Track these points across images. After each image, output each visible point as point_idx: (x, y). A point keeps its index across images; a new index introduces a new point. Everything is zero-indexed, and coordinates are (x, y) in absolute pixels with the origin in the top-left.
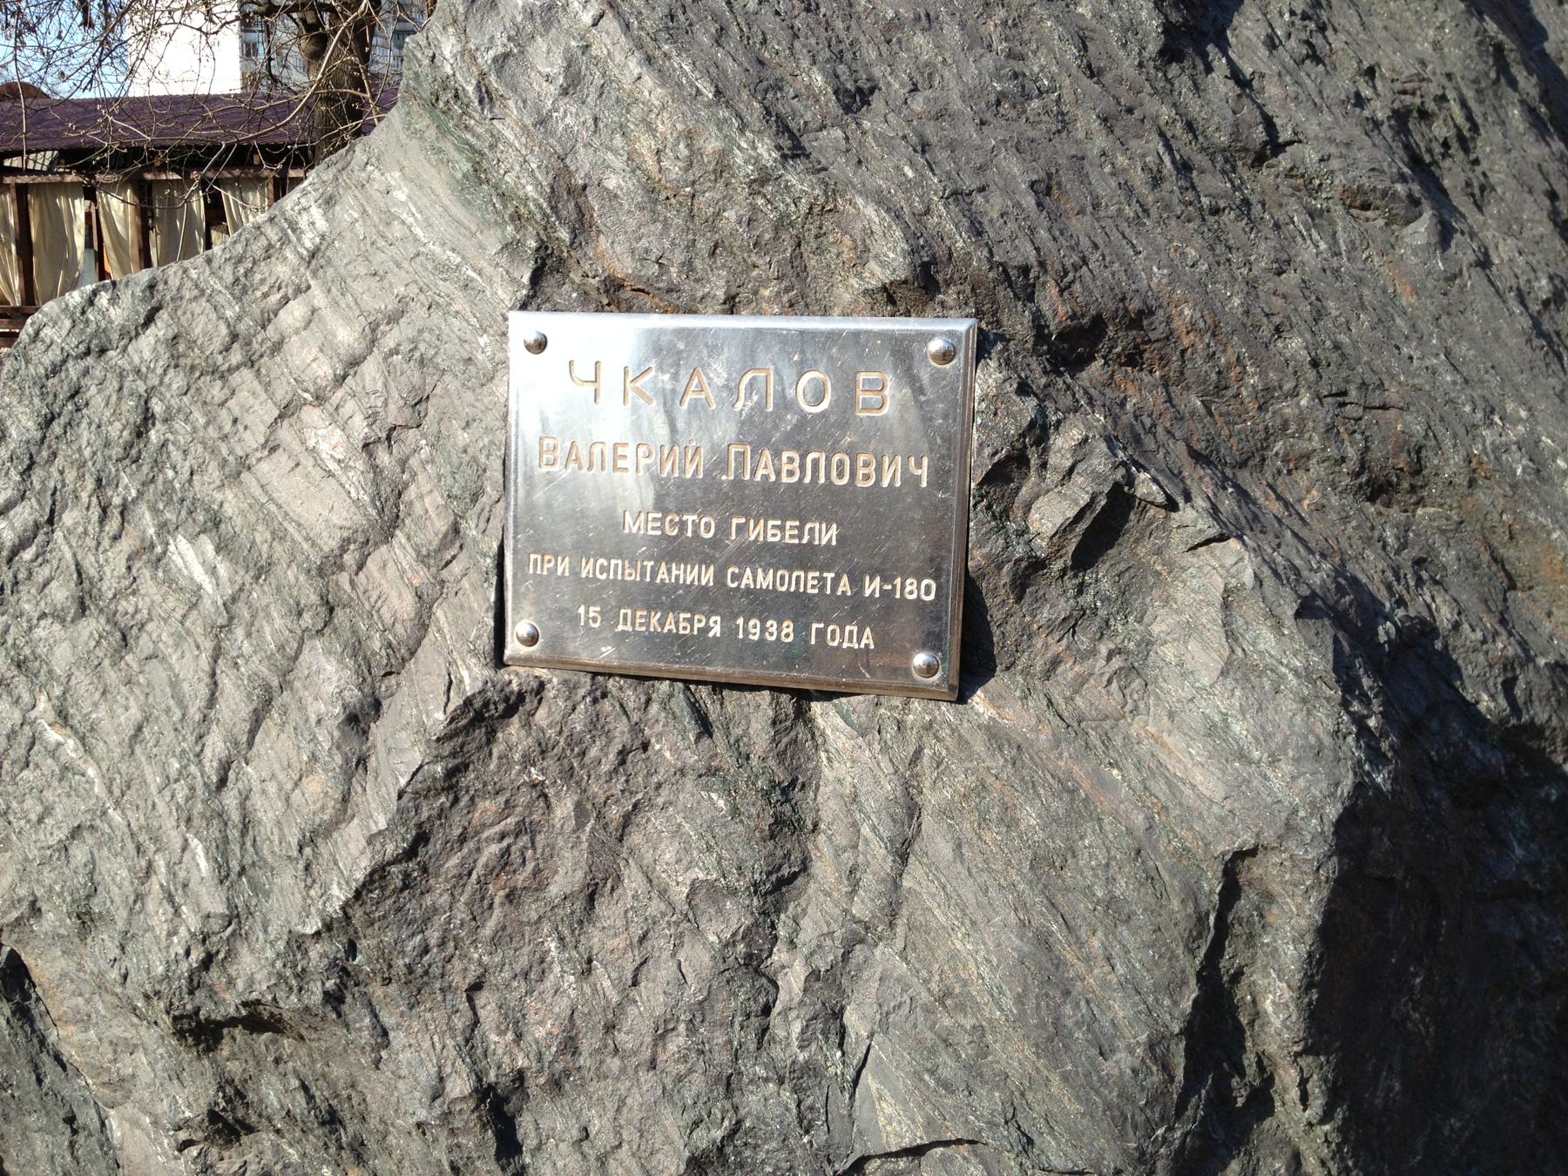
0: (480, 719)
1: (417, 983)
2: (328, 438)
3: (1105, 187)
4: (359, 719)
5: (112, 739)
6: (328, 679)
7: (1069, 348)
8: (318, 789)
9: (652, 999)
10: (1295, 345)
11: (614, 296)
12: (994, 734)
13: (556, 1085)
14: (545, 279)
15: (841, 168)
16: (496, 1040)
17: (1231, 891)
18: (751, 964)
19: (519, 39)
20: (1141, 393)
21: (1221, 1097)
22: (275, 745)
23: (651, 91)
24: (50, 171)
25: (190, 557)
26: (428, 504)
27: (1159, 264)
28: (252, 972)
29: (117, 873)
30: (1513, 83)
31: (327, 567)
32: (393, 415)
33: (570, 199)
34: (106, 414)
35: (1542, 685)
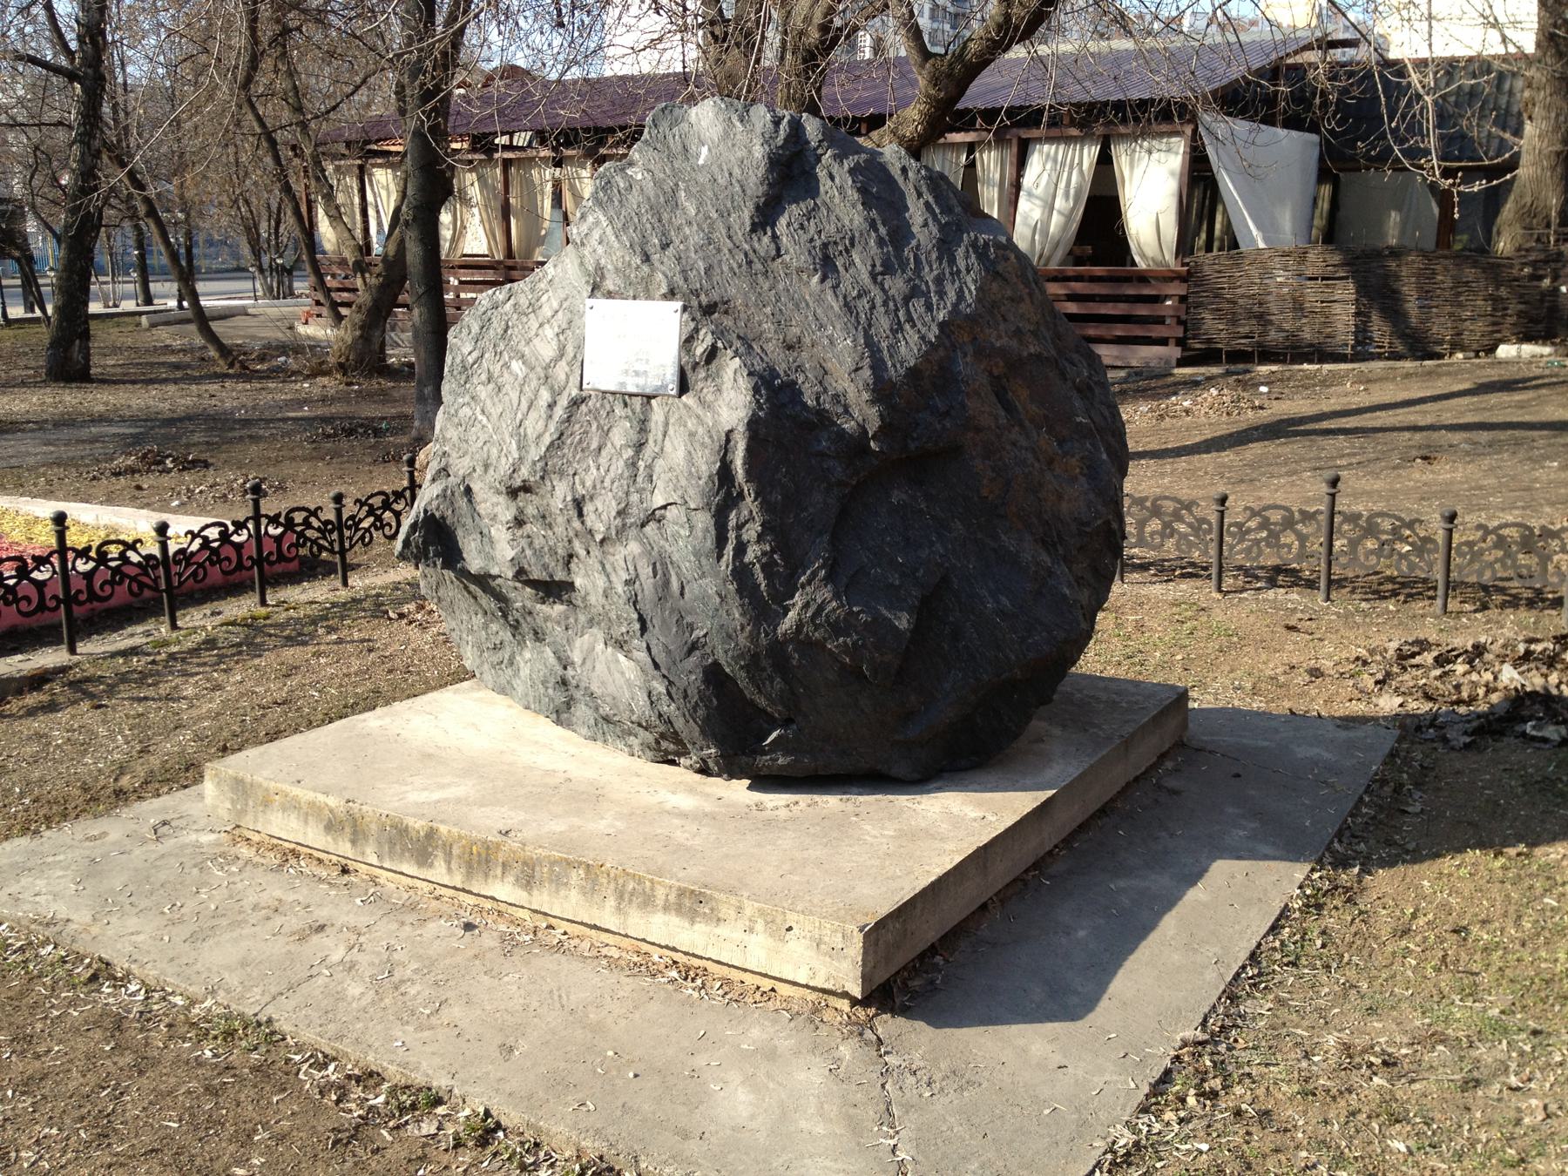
0: (576, 403)
1: (561, 473)
2: (549, 332)
3: (725, 268)
4: (551, 406)
5: (495, 416)
6: (545, 396)
7: (709, 310)
8: (541, 423)
9: (612, 474)
10: (768, 310)
11: (610, 295)
12: (685, 405)
13: (591, 498)
14: (595, 289)
15: (657, 264)
16: (579, 487)
17: (728, 440)
18: (633, 464)
19: (590, 229)
20: (728, 322)
21: (729, 493)
22: (533, 415)
23: (616, 245)
24: (530, 145)
25: (516, 366)
26: (570, 350)
27: (735, 290)
28: (524, 472)
29: (494, 451)
30: (876, 230)
31: (546, 368)
32: (564, 326)
33: (600, 271)
34: (497, 327)
35: (828, 399)
